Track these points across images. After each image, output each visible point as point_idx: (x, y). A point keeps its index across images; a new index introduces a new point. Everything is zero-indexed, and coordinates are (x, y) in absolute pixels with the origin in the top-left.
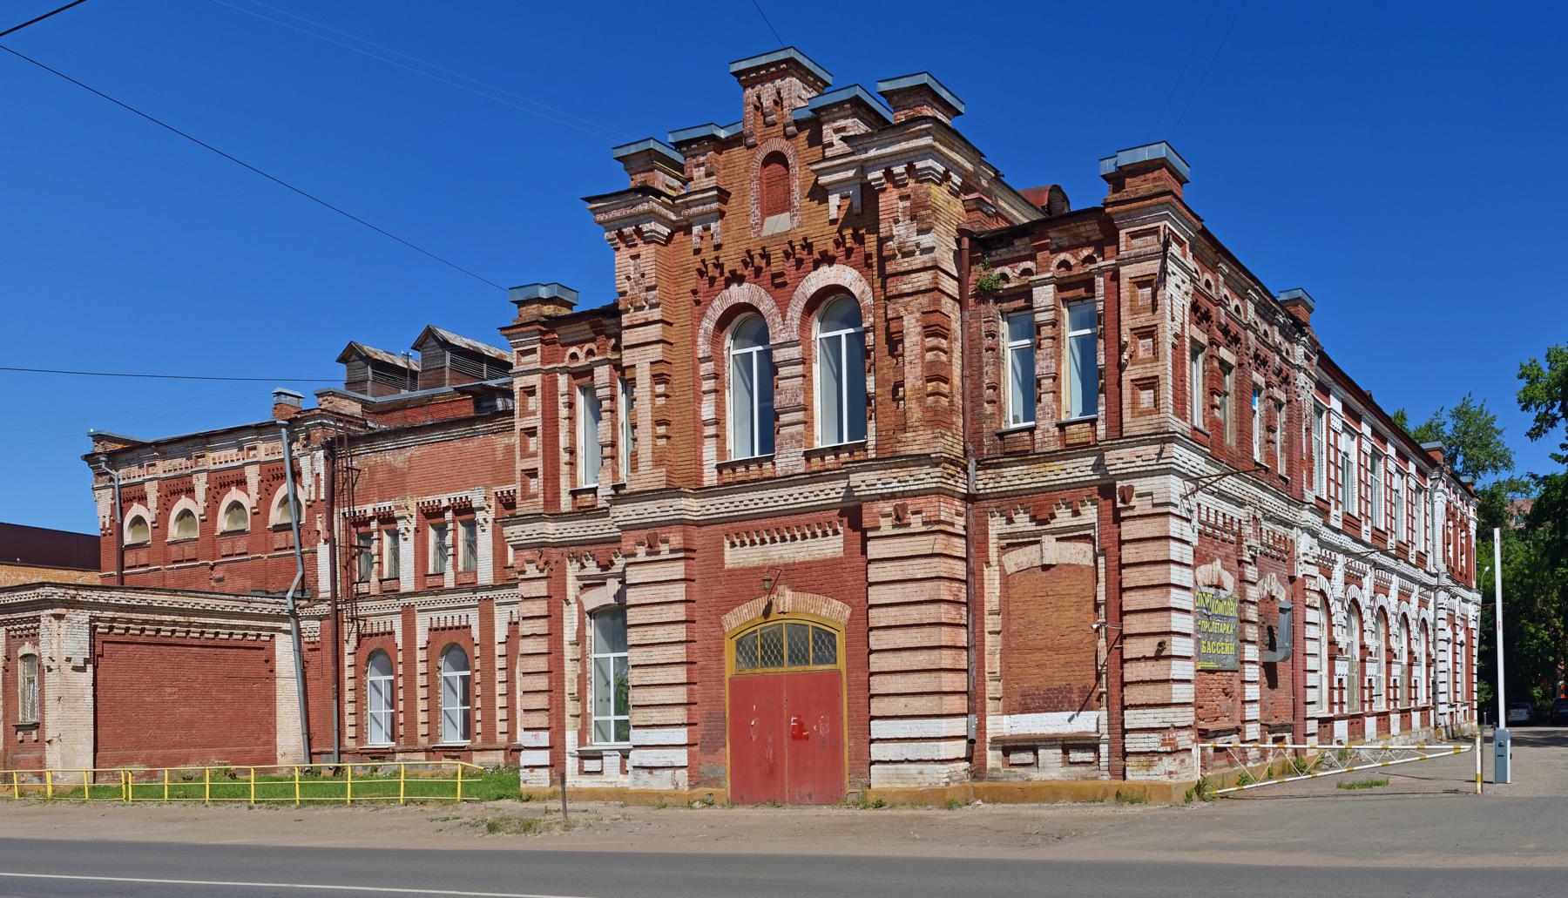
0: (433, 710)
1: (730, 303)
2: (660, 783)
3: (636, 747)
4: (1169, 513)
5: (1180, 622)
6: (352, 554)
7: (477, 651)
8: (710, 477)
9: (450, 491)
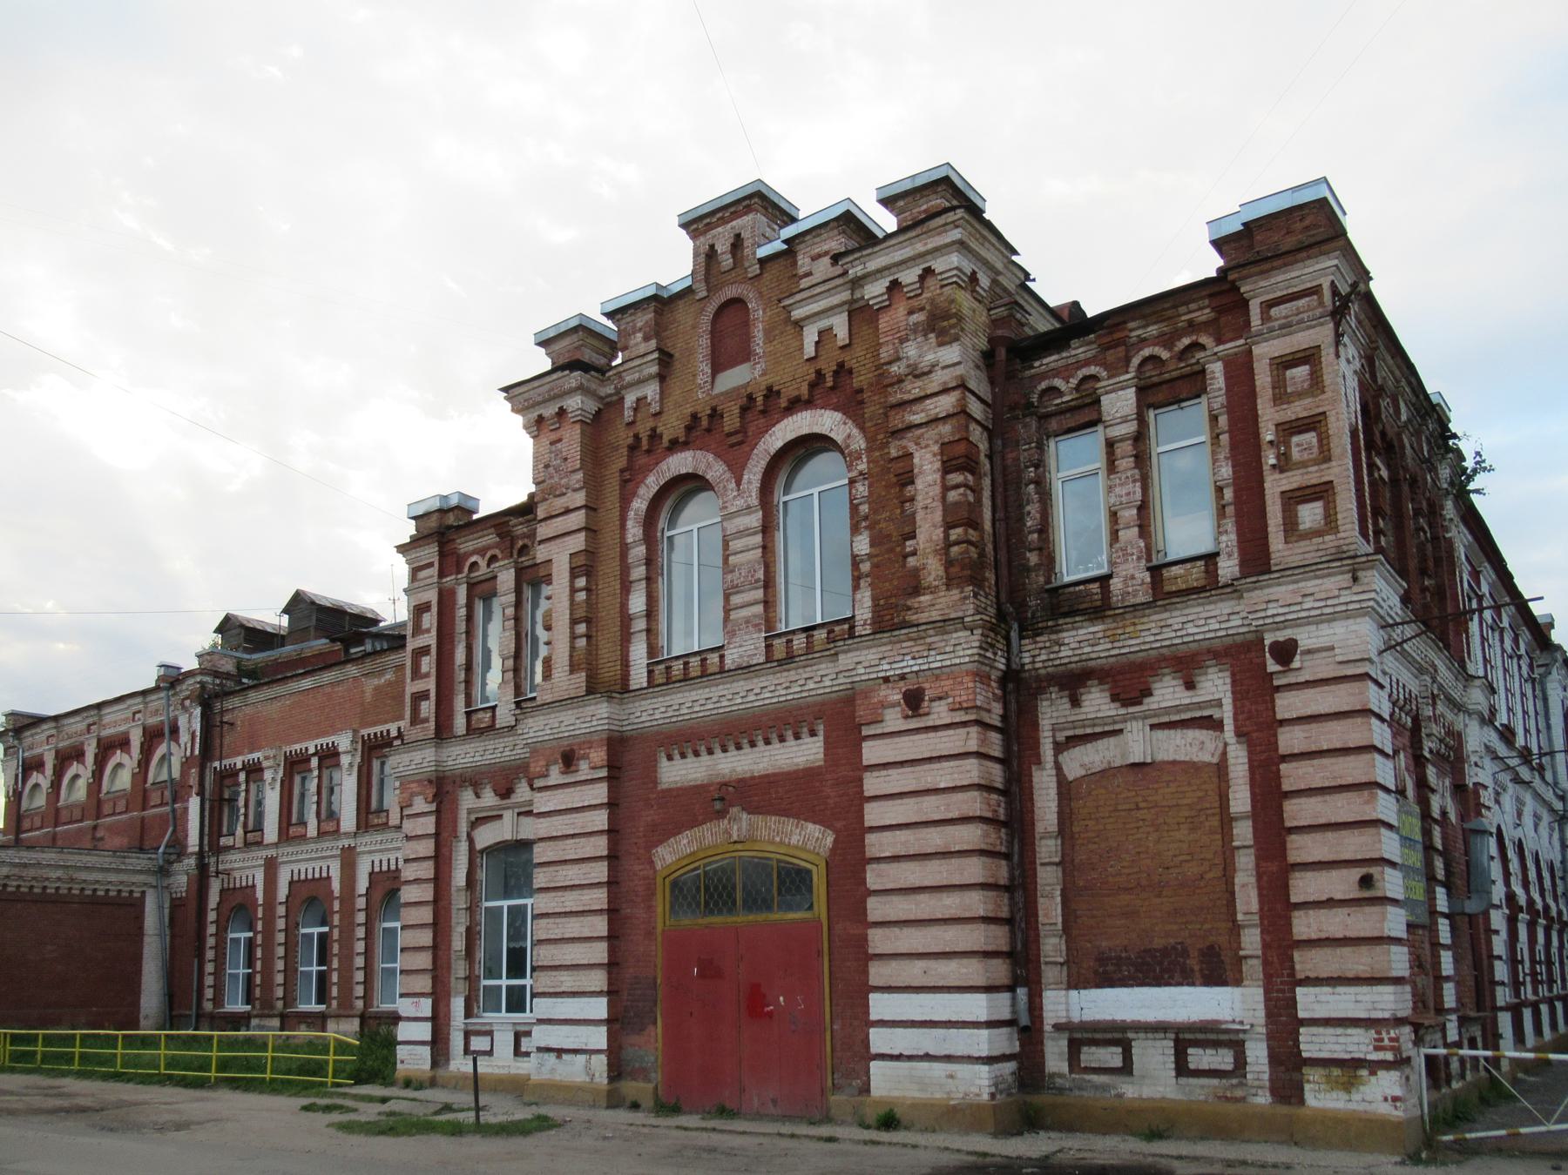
0: (290, 971)
1: (668, 476)
2: (573, 1071)
3: (541, 1021)
4: (1367, 676)
5: (1390, 845)
6: (219, 806)
7: (336, 907)
9: (318, 737)
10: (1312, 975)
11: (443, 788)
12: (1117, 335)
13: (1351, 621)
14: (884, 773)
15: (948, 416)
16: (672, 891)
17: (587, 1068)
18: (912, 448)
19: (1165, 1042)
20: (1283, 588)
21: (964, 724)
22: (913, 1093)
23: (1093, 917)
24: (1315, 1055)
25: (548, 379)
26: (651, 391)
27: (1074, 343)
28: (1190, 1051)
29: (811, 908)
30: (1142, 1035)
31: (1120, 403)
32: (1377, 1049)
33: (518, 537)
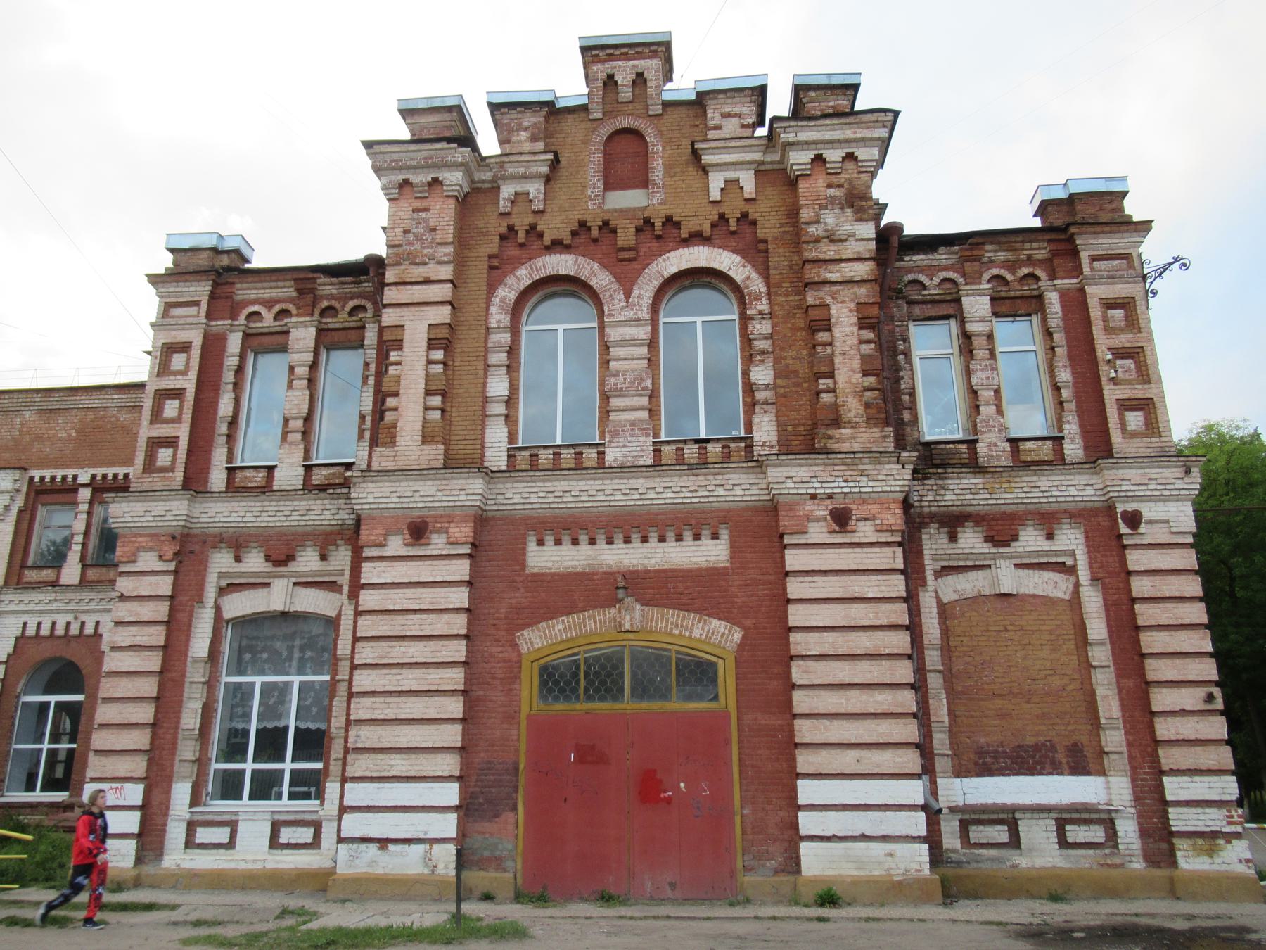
1: (543, 274)
8: (497, 457)
10: (1175, 767)
11: (187, 550)
12: (976, 252)
13: (1180, 503)
14: (809, 579)
15: (863, 281)
16: (541, 676)
17: (427, 859)
18: (829, 300)
19: (1047, 821)
20: (1134, 471)
21: (888, 544)
22: (850, 871)
23: (972, 717)
24: (1183, 829)
25: (404, 147)
26: (535, 189)
27: (942, 249)
28: (1068, 828)
29: (716, 698)
30: (1028, 815)
31: (303, 336)
32: (1229, 823)
33: (322, 297)
